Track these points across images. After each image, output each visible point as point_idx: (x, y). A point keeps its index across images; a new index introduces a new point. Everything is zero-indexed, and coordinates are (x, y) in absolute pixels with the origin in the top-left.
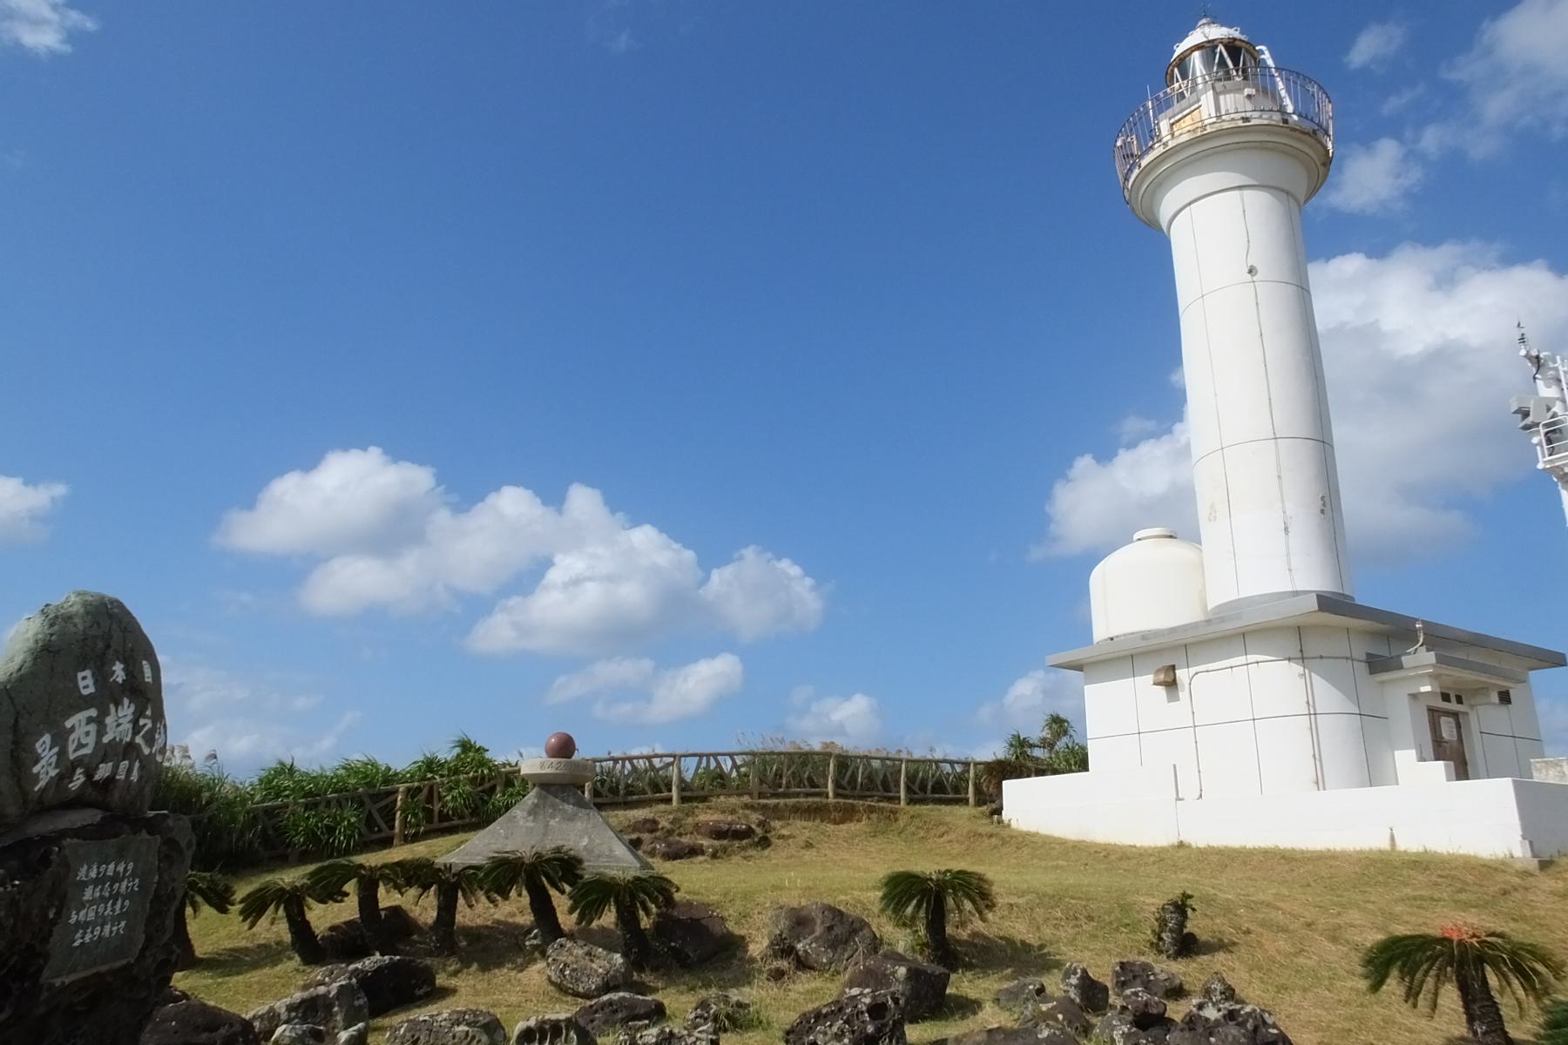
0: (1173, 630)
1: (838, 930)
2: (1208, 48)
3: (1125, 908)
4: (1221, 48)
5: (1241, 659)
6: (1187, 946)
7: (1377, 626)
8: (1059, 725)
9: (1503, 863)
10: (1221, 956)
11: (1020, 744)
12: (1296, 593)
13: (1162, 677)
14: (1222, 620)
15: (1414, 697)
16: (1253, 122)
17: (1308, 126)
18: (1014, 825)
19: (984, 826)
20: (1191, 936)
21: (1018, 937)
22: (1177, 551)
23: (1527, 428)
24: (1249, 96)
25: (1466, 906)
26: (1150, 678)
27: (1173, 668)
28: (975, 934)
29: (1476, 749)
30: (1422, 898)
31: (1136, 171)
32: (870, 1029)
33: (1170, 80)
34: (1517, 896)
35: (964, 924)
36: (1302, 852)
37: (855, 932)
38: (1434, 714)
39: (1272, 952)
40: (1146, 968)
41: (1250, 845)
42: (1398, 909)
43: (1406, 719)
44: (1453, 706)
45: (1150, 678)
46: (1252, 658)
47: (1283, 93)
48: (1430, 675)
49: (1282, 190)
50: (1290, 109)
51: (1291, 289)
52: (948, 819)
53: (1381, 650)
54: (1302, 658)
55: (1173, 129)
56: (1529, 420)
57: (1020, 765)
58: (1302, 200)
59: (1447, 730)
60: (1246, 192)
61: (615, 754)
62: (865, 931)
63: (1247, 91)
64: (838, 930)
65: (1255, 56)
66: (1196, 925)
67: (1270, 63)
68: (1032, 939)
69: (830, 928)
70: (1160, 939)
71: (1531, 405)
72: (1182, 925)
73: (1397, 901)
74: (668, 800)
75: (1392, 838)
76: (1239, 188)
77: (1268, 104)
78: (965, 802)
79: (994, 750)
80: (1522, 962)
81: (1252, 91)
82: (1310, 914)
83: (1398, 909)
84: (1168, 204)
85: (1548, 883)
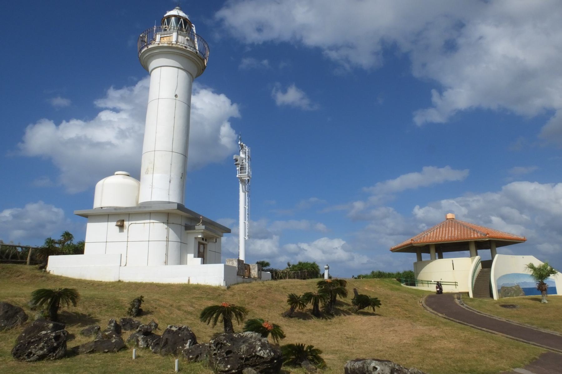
0: (127, 208)
1: (10, 313)
2: (178, 18)
3: (117, 301)
4: (182, 19)
5: (148, 221)
6: (140, 313)
7: (191, 216)
8: (68, 236)
9: (218, 287)
10: (149, 316)
11: (50, 242)
12: (169, 202)
13: (119, 223)
14: (145, 207)
15: (196, 238)
16: (188, 49)
17: (202, 56)
18: (51, 273)
19: (38, 273)
20: (141, 310)
21: (80, 312)
22: (131, 181)
23: (236, 164)
24: (187, 40)
25: (210, 299)
26: (115, 223)
27: (123, 221)
28: (64, 312)
29: (208, 254)
30: (199, 297)
31: (146, 49)
32: (55, 344)
33: (162, 23)
34: (222, 296)
35: (66, 308)
36: (163, 284)
37: (17, 313)
38: (200, 243)
39: (164, 314)
40: (131, 320)
41: (144, 282)
42: (194, 300)
43: (192, 245)
44: (204, 242)
45: (115, 223)
46: (152, 221)
47: (196, 42)
48: (202, 232)
49: (191, 75)
50: (197, 48)
51: (186, 105)
52: (21, 270)
53: (189, 223)
54: (167, 223)
55: (160, 40)
56: (237, 162)
57: (52, 249)
58: (194, 77)
59: (202, 250)
60: (180, 70)
61: (21, 245)
62: (21, 313)
63: (187, 38)
64: (10, 313)
65: (191, 27)
66: (143, 306)
67: (195, 31)
68: (85, 312)
69: (7, 312)
70: (132, 311)
71: (239, 158)
72: (139, 306)
73: (193, 298)
74: (25, 263)
75: (189, 280)
76: (178, 68)
77: (191, 44)
78: (25, 263)
79: (41, 244)
80: (240, 312)
81: (189, 39)
82: (171, 303)
83: (194, 300)
84: (153, 64)
85: (229, 293)
